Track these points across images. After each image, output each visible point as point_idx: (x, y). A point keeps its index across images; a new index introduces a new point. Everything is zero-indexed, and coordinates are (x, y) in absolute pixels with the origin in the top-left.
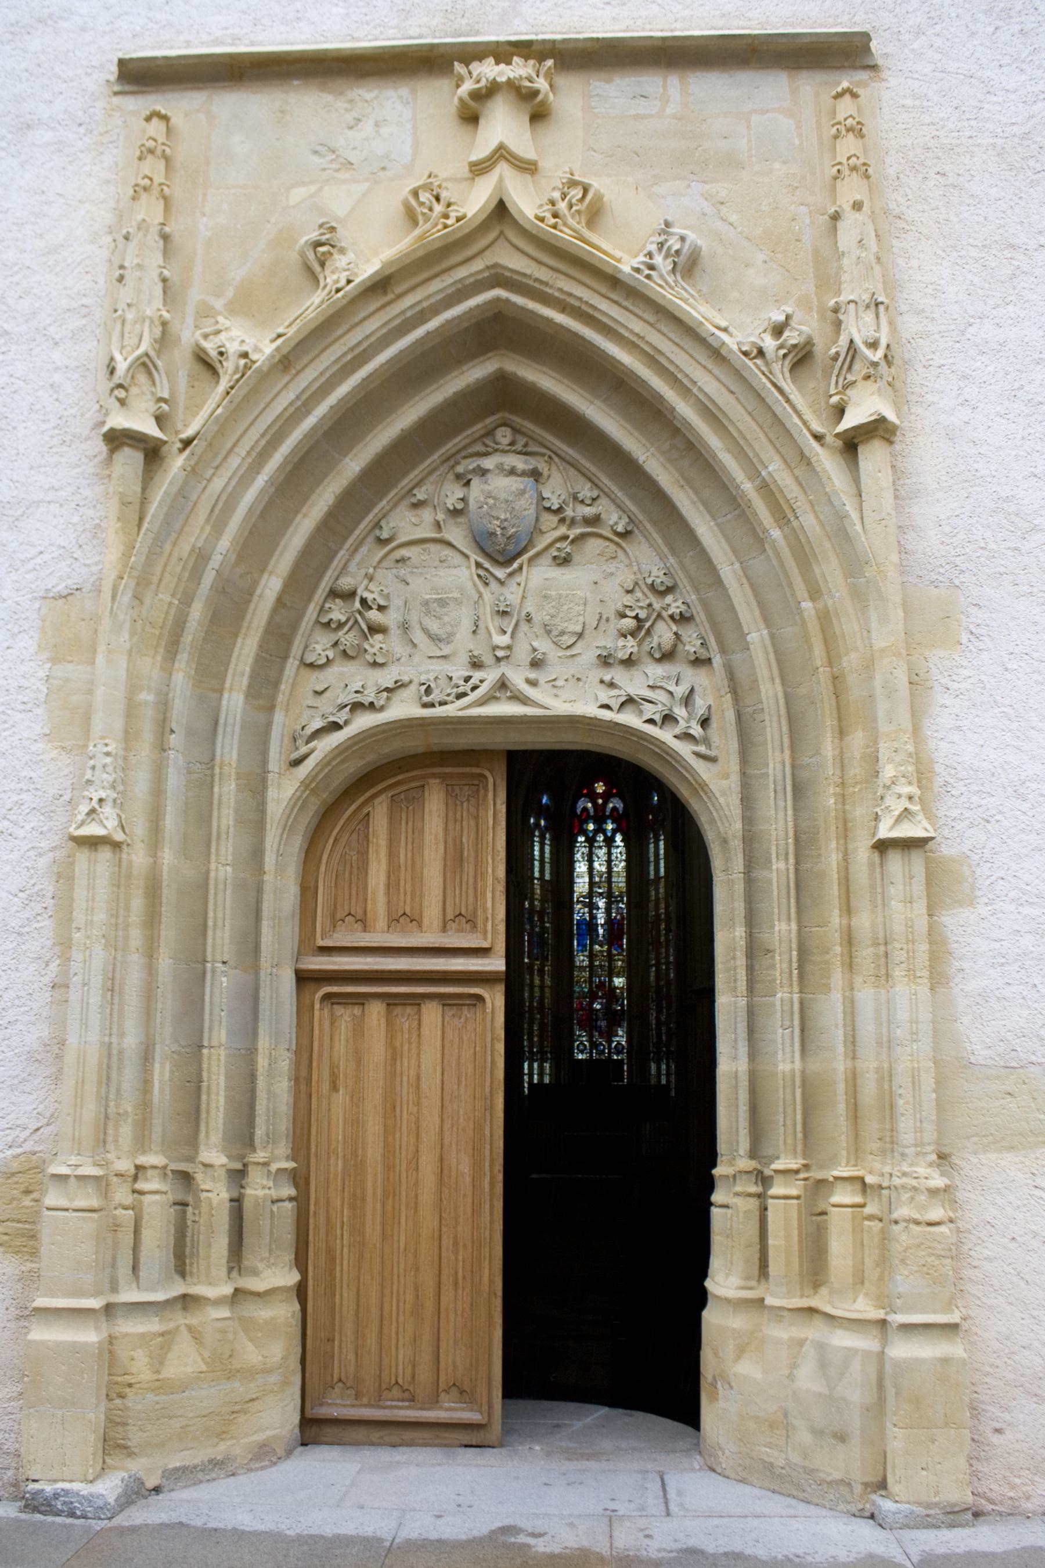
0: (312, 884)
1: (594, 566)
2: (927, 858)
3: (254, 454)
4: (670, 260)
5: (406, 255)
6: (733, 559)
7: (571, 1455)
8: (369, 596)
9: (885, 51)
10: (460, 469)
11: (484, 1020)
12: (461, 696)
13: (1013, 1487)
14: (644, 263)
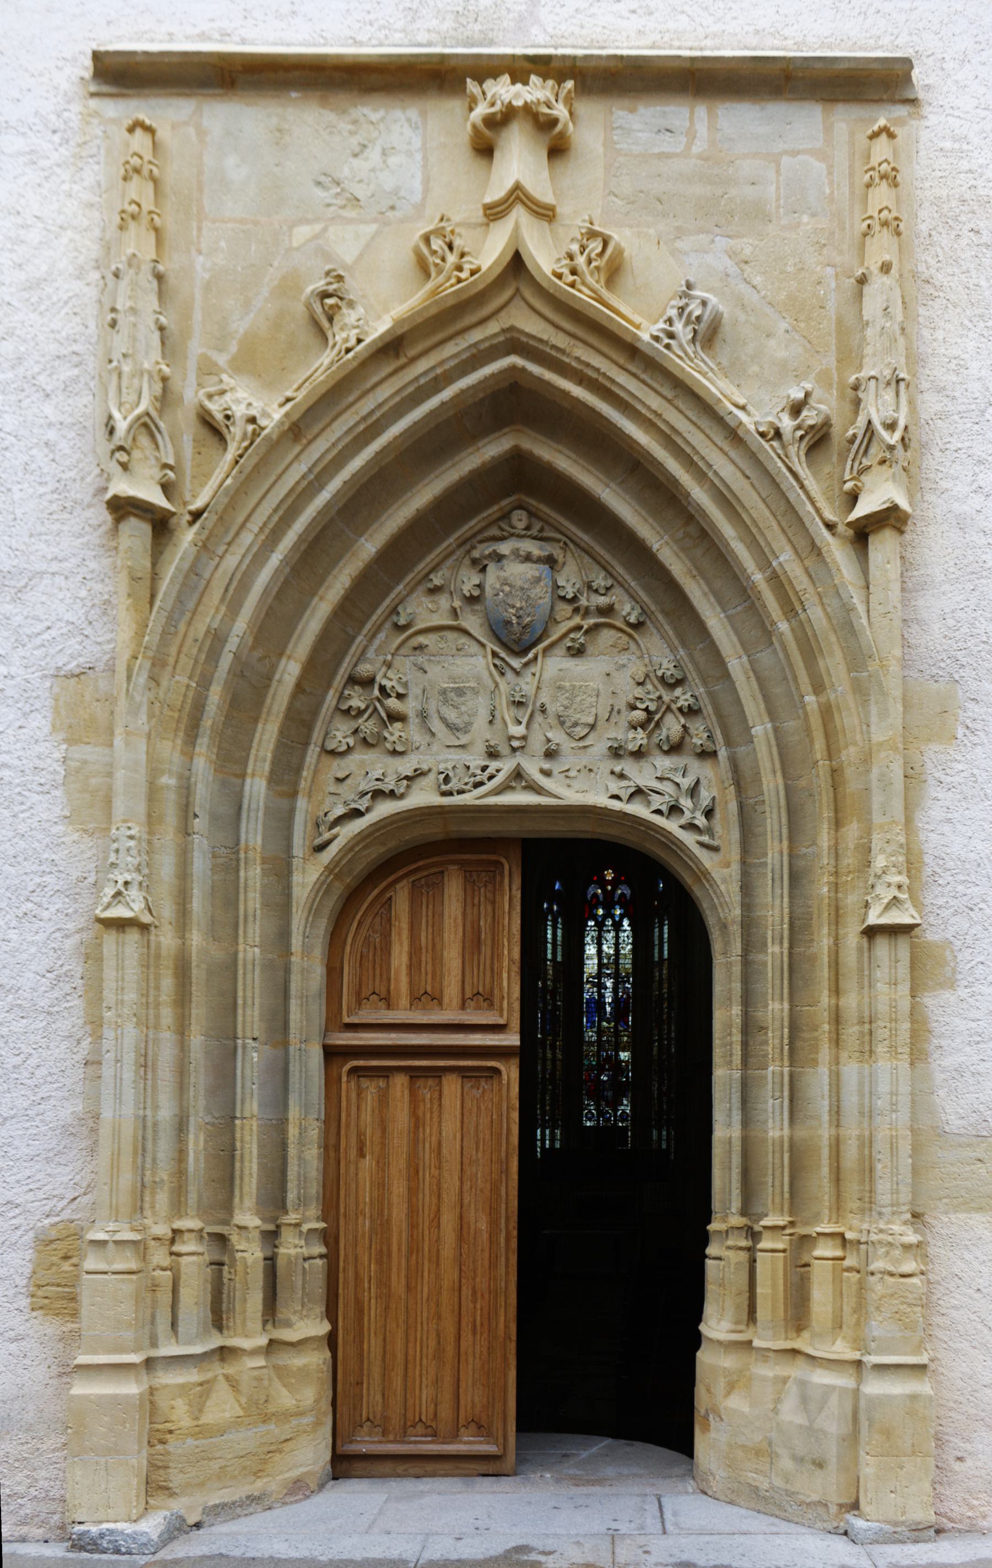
0: (338, 965)
1: (607, 658)
2: (912, 943)
3: (267, 531)
4: (690, 327)
5: (419, 313)
6: (741, 652)
7: (578, 1481)
8: (388, 684)
9: (926, 82)
10: (476, 554)
11: (500, 1090)
12: (478, 785)
13: (971, 1508)
14: (664, 331)
